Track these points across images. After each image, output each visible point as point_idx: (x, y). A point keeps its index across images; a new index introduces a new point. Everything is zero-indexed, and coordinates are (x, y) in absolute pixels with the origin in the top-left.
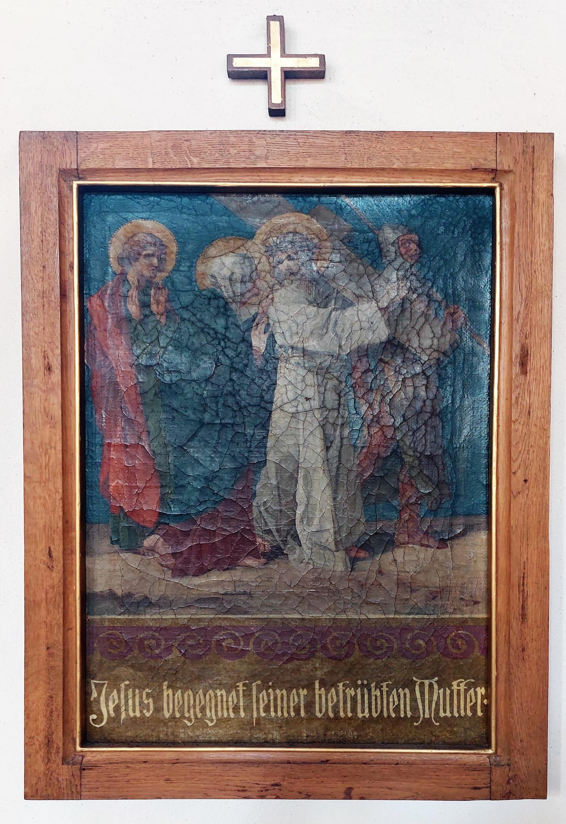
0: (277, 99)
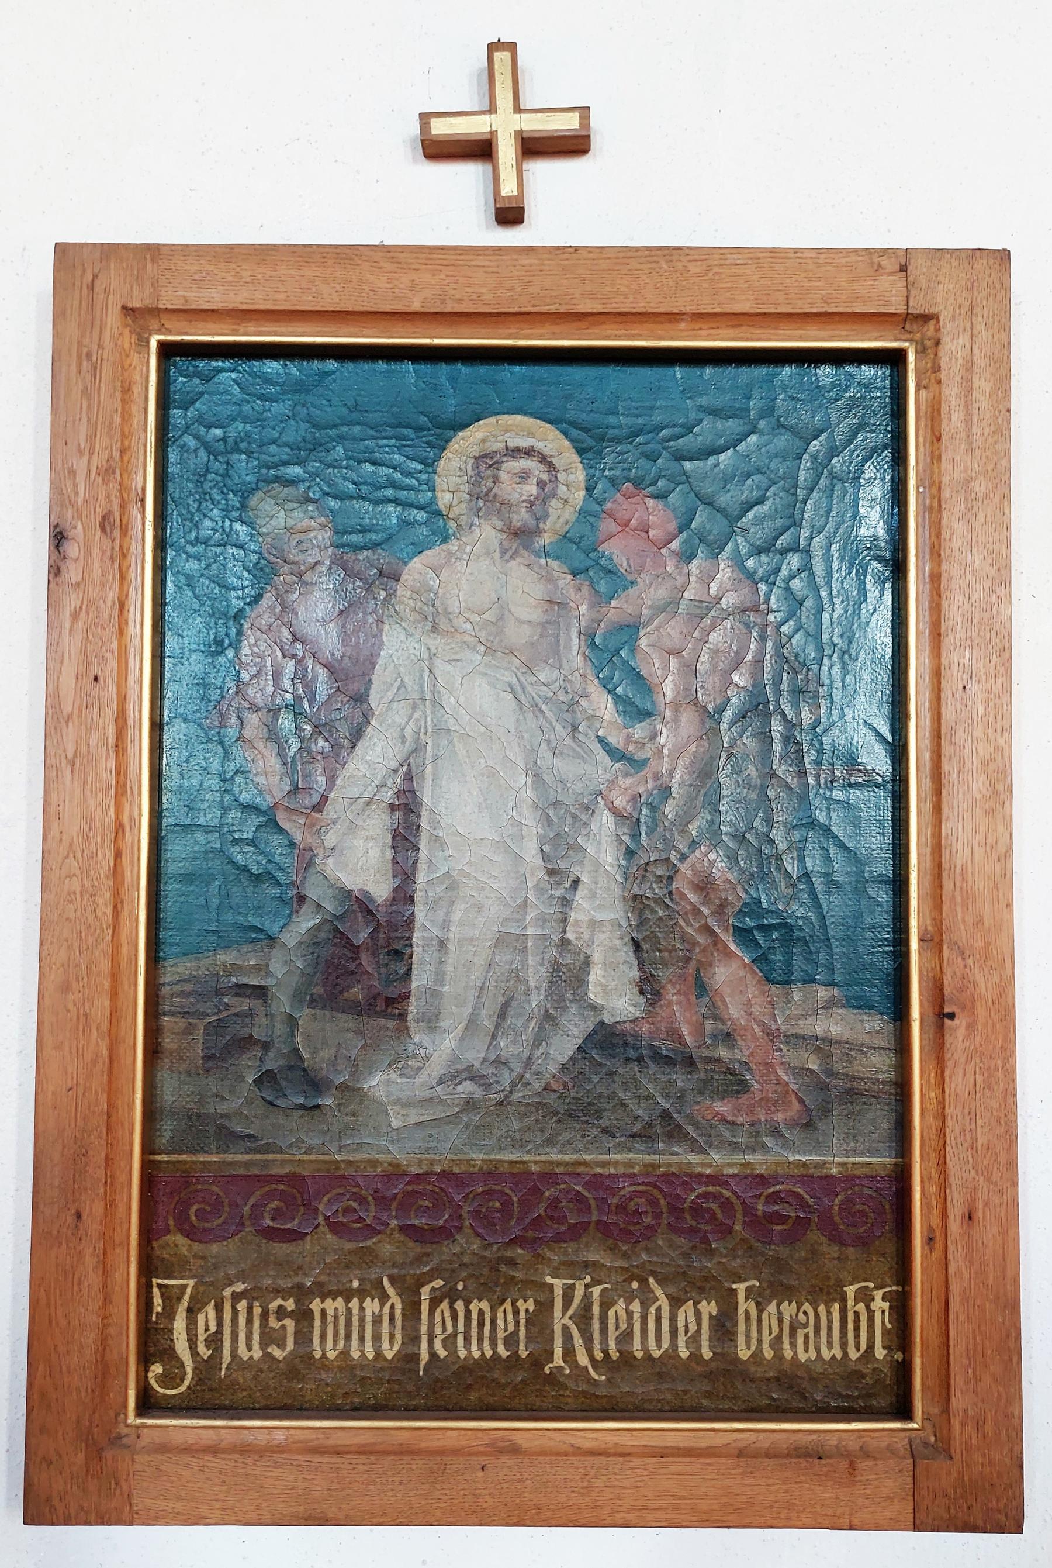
0: (509, 188)
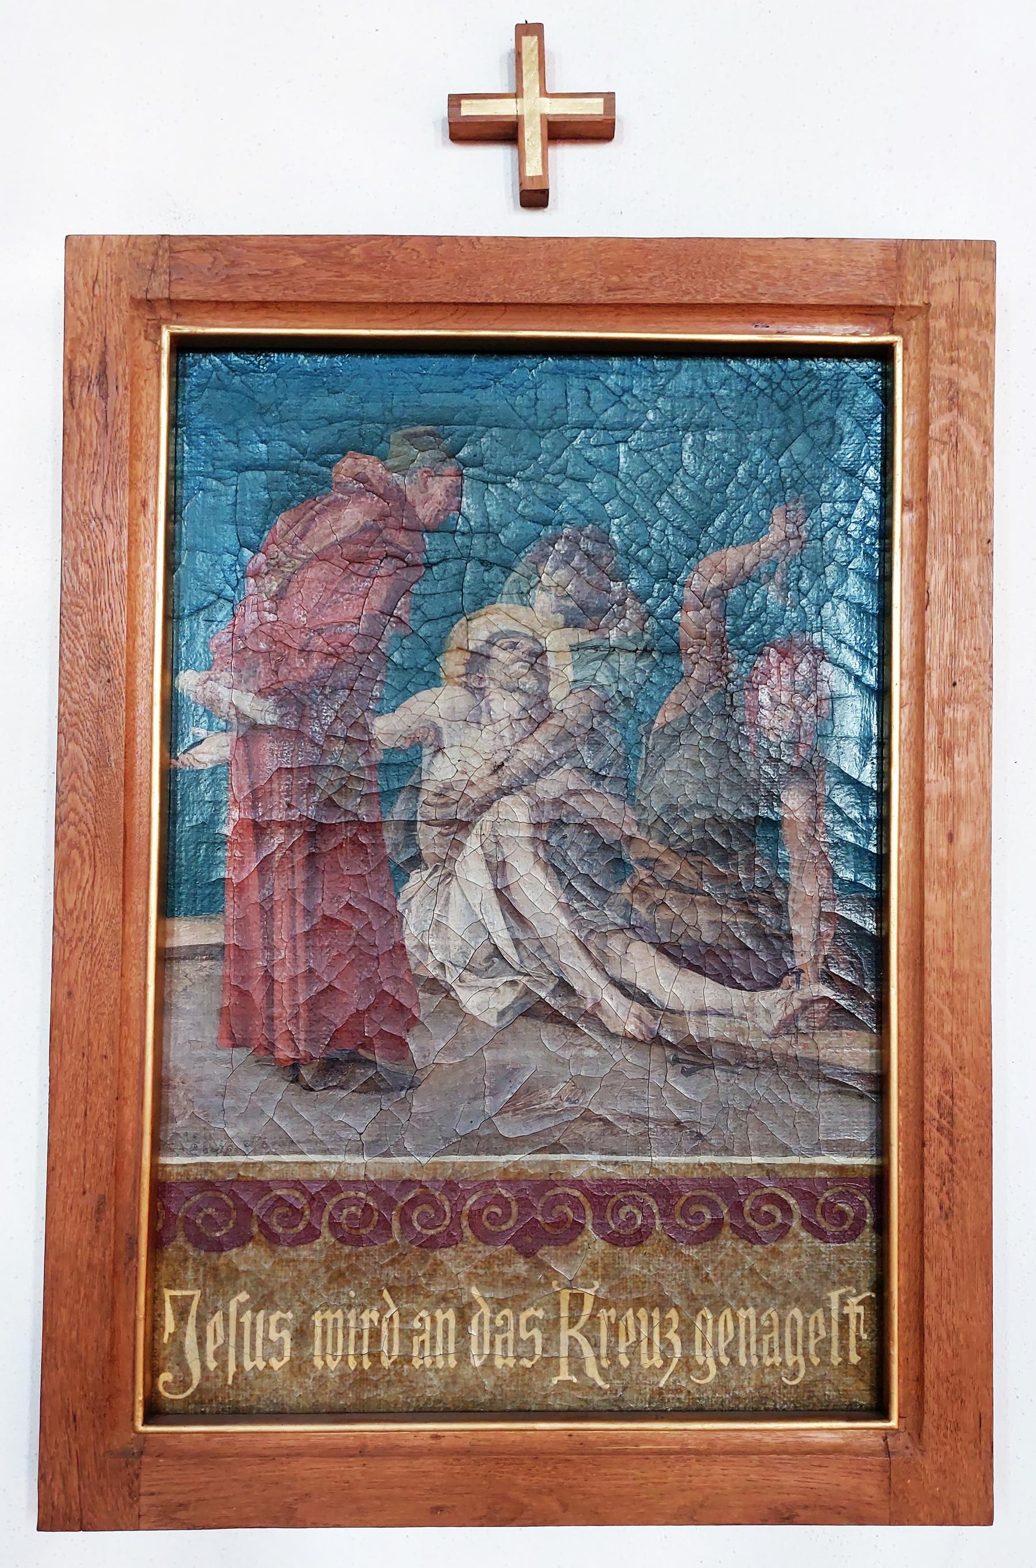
0: (533, 168)
